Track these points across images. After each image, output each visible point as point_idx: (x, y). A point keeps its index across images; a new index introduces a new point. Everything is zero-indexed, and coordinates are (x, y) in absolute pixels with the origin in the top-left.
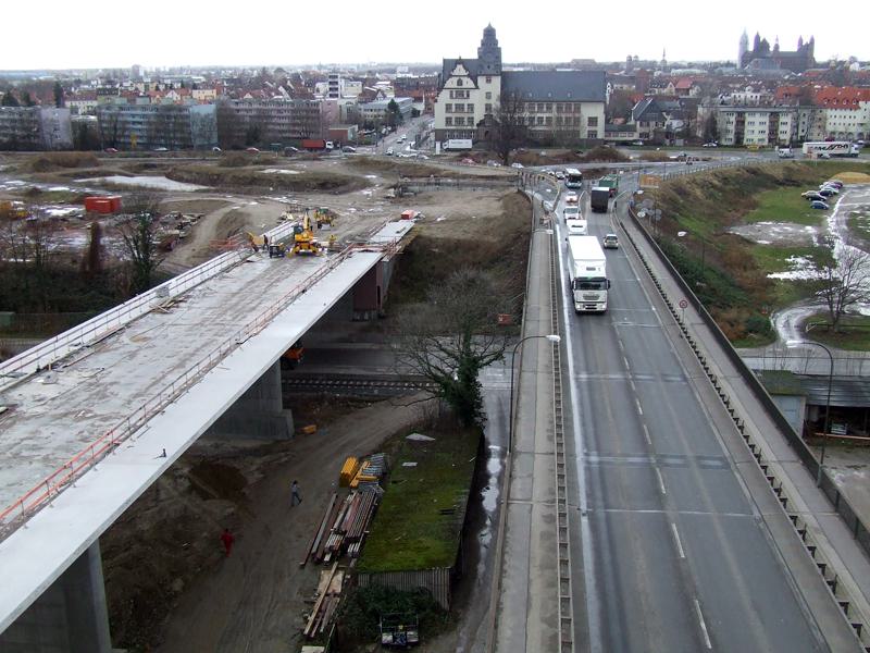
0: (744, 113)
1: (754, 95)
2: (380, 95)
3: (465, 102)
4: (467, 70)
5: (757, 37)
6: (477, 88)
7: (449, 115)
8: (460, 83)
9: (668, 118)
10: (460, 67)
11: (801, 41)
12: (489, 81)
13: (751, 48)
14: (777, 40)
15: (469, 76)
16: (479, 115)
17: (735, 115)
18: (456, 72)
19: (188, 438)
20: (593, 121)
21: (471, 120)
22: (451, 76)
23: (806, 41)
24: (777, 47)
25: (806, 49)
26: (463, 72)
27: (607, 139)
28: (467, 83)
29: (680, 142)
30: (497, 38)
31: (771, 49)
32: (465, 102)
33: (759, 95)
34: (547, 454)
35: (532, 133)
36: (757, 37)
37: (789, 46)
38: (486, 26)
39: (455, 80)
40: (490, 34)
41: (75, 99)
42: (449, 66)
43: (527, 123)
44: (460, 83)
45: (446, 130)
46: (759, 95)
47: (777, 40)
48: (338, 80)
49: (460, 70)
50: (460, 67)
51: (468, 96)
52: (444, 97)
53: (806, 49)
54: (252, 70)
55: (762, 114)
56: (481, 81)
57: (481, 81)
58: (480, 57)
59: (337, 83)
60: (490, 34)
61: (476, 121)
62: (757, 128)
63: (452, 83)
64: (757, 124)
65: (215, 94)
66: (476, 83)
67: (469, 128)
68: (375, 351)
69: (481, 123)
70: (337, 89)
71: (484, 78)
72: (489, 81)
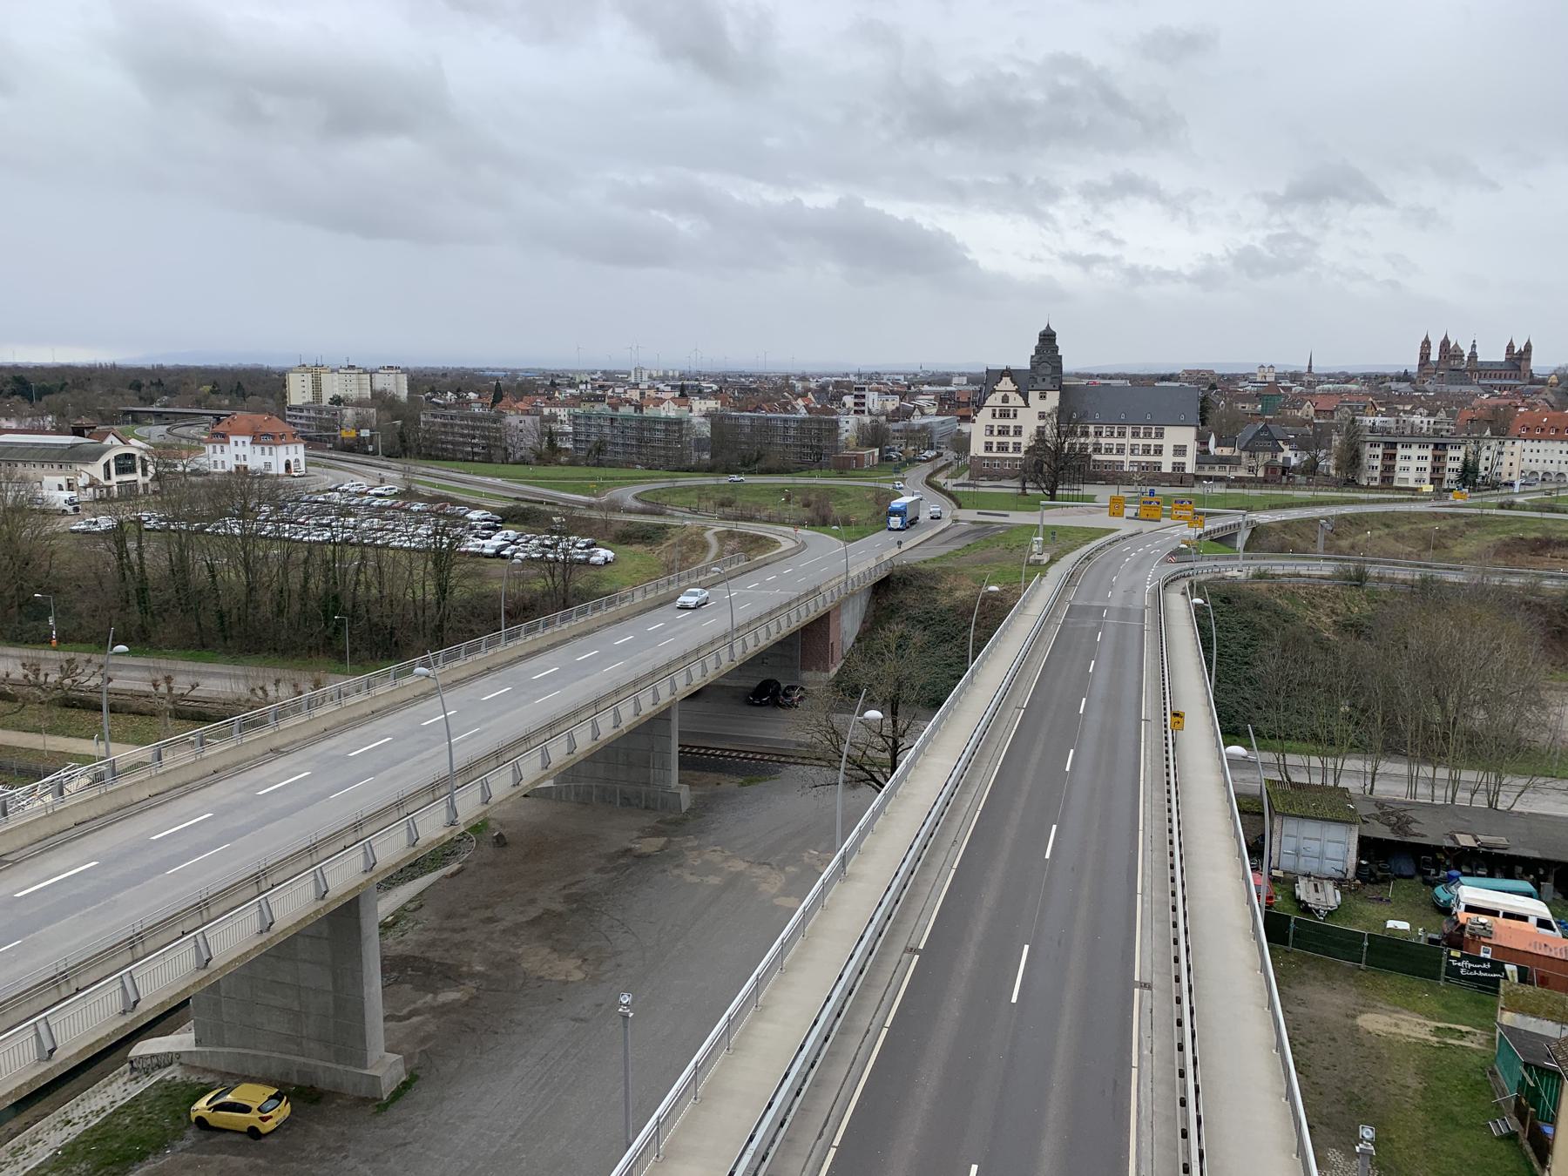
0: (1396, 443)
1: (1426, 420)
2: (917, 412)
3: (1011, 423)
4: (1015, 383)
5: (1445, 343)
6: (1027, 405)
8: (1005, 399)
9: (1286, 448)
10: (1006, 380)
11: (1511, 347)
12: (1043, 397)
13: (1434, 356)
14: (1474, 346)
15: (1017, 391)
16: (1026, 441)
17: (1431, 447)
18: (1000, 386)
19: (24, 361)
20: (1180, 450)
21: (1017, 448)
22: (994, 391)
24: (1473, 355)
25: (1518, 359)
26: (1011, 386)
27: (1199, 473)
28: (1015, 400)
29: (1300, 478)
33: (1432, 420)
34: (621, 952)
35: (1098, 463)
36: (1445, 343)
37: (1492, 353)
38: (1044, 328)
39: (999, 395)
40: (1048, 338)
41: (556, 405)
42: (992, 377)
43: (1090, 450)
44: (1005, 399)
45: (985, 458)
46: (1432, 420)
47: (1474, 346)
48: (866, 393)
49: (1006, 384)
50: (1006, 380)
51: (1015, 415)
52: (984, 417)
53: (1518, 359)
54: (685, 390)
55: (1422, 446)
56: (1034, 396)
57: (1034, 396)
58: (1032, 367)
59: (864, 396)
60: (1048, 338)
62: (1414, 464)
63: (994, 400)
64: (1414, 457)
65: (719, 406)
68: (642, 857)
69: (1030, 450)
70: (863, 404)
71: (1037, 394)
72: (1043, 397)
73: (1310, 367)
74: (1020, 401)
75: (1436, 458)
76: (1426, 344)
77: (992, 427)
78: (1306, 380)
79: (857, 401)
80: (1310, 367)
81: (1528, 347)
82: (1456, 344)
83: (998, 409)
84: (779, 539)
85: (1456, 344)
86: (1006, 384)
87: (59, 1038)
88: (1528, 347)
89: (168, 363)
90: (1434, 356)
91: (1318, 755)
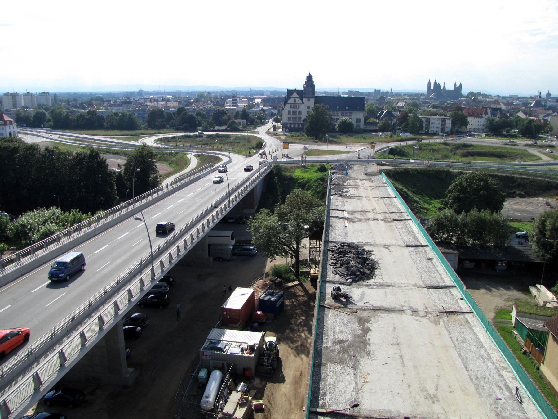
3: (297, 110)
5: (435, 83)
6: (303, 103)
7: (289, 116)
8: (295, 101)
11: (455, 85)
12: (309, 100)
13: (432, 88)
14: (445, 84)
15: (299, 98)
23: (458, 85)
24: (444, 87)
25: (458, 89)
28: (299, 101)
30: (313, 80)
31: (437, 84)
32: (297, 110)
36: (435, 83)
37: (450, 87)
39: (293, 100)
40: (310, 78)
44: (295, 101)
47: (445, 84)
49: (295, 95)
53: (458, 89)
56: (305, 100)
59: (236, 100)
61: (302, 119)
63: (291, 101)
66: (303, 102)
67: (299, 122)
72: (309, 100)
73: (392, 90)
74: (300, 102)
75: (429, 128)
76: (429, 83)
77: (290, 111)
78: (391, 94)
79: (233, 101)
80: (392, 90)
81: (461, 85)
82: (439, 84)
83: (292, 105)
84: (221, 157)
85: (439, 84)
86: (295, 94)
87: (10, 405)
88: (461, 85)
89: (190, 91)
90: (432, 88)
91: (307, 347)
